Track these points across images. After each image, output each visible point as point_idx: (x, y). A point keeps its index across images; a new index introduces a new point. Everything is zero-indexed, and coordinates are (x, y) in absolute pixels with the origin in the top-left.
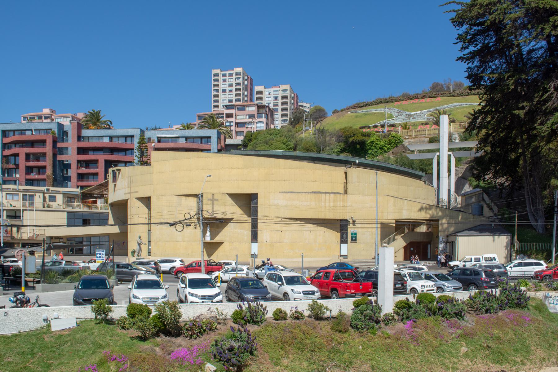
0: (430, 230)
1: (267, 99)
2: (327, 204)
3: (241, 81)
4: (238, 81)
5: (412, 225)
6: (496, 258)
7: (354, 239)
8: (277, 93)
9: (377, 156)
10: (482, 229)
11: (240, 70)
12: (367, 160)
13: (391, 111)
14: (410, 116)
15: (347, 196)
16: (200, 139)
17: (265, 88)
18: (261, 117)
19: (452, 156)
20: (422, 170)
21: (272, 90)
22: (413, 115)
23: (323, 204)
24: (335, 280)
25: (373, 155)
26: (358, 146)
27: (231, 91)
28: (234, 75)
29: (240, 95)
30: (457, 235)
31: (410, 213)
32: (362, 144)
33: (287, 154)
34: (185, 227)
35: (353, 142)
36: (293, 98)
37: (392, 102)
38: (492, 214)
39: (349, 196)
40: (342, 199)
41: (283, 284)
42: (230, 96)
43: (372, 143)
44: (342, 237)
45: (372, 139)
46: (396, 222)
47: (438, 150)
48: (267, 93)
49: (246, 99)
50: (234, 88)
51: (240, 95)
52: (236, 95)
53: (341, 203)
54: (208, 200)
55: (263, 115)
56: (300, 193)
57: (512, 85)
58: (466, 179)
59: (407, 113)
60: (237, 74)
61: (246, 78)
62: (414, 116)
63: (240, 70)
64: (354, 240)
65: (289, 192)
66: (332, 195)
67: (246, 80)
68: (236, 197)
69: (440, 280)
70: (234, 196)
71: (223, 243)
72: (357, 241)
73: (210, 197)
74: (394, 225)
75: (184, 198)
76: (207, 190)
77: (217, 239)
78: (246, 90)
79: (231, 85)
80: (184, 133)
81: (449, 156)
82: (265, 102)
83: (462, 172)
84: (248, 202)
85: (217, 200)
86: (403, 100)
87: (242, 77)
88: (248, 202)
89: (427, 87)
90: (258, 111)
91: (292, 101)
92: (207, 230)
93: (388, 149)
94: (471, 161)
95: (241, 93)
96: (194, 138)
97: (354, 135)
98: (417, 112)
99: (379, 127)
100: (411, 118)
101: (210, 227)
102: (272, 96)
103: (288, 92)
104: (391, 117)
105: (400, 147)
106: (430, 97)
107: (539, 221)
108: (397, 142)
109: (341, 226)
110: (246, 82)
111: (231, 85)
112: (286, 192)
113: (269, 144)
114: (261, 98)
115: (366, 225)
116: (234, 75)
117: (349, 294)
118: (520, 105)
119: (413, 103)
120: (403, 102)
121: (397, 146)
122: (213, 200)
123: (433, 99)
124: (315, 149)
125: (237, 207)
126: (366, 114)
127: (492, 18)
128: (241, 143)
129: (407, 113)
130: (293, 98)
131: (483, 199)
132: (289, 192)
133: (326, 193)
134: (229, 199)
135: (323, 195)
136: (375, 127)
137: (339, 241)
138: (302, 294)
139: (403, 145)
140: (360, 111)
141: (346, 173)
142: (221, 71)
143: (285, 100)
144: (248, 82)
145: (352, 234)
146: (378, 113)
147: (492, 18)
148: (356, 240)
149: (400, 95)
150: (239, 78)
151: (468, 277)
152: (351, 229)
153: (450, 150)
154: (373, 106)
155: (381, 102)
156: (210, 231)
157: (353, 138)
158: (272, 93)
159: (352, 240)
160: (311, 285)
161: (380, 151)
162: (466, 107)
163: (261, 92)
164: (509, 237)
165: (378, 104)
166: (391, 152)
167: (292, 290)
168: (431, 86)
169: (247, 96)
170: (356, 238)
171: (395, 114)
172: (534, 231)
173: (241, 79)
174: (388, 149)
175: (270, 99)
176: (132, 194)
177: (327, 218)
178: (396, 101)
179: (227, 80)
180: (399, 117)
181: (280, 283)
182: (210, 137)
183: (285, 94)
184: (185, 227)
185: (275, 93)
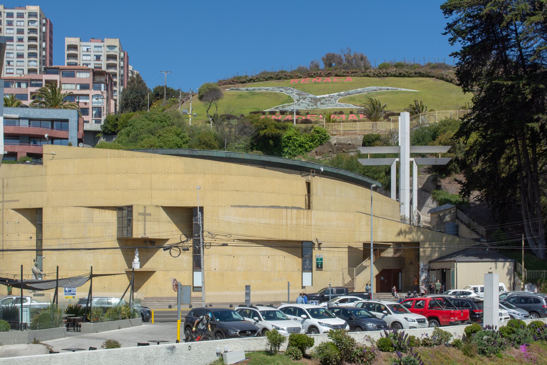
0: (398, 255)
1: (85, 58)
2: (289, 222)
3: (36, 26)
4: (32, 26)
5: (380, 247)
6: (504, 287)
7: (320, 266)
8: (100, 49)
9: (295, 156)
10: (478, 253)
11: (35, 9)
12: (285, 160)
13: (288, 91)
14: (316, 101)
15: (311, 212)
16: (50, 122)
17: (81, 41)
18: (100, 89)
19: (414, 163)
20: (379, 180)
21: (92, 44)
22: (320, 100)
23: (284, 222)
24: (430, 308)
25: (290, 154)
26: (271, 142)
27: (21, 40)
28: (26, 16)
29: (35, 47)
30: (455, 261)
31: (388, 233)
32: (277, 139)
33: (232, 156)
34: (182, 251)
35: (265, 135)
36: (122, 59)
37: (286, 79)
38: (475, 236)
39: (314, 213)
40: (305, 215)
41: (260, 319)
42: (19, 48)
43: (289, 138)
44: (303, 264)
45: (289, 133)
46: (364, 244)
47: (397, 155)
48: (85, 49)
49: (44, 53)
50: (26, 36)
51: (35, 47)
52: (30, 47)
53: (305, 221)
54: (139, 214)
55: (103, 85)
56: (256, 207)
57: (529, 94)
58: (429, 192)
59: (311, 96)
60: (30, 15)
61: (44, 21)
62: (322, 101)
63: (35, 9)
64: (320, 267)
65: (242, 206)
66: (295, 211)
67: (44, 25)
68: (173, 212)
69: (313, 317)
70: (169, 210)
71: (153, 272)
72: (324, 269)
73: (141, 210)
74: (362, 249)
75: (98, 210)
76: (138, 203)
77: (148, 266)
78: (44, 41)
79: (20, 31)
80: (26, 113)
81: (411, 163)
82: (82, 63)
83: (423, 183)
84: (188, 218)
85: (150, 215)
86: (300, 77)
87: (38, 19)
88: (188, 218)
89: (316, 57)
90: (94, 80)
91: (122, 63)
92: (134, 255)
93: (310, 147)
94: (429, 169)
95: (38, 44)
96: (40, 120)
97: (266, 126)
98: (325, 96)
99: (278, 113)
100: (319, 103)
101: (139, 251)
102: (92, 54)
103: (117, 49)
104: (290, 100)
105: (325, 145)
106: (336, 76)
107: (540, 245)
108: (321, 139)
109: (302, 249)
110: (44, 29)
111: (20, 31)
112: (239, 206)
113: (157, 135)
114: (75, 56)
115: (332, 249)
116: (26, 16)
117: (452, 321)
118: (536, 117)
119: (315, 83)
120: (302, 80)
121: (321, 144)
122: (145, 214)
123: (343, 79)
124: (216, 144)
125: (173, 224)
126: (253, 94)
127: (509, 18)
128: (100, 129)
129: (311, 96)
130: (122, 59)
131: (457, 218)
132: (242, 206)
133: (286, 208)
134: (164, 215)
135: (284, 210)
136: (273, 113)
137: (301, 270)
138: (416, 322)
139: (329, 143)
140: (243, 89)
141: (308, 184)
142: (5, 8)
143: (111, 62)
144: (46, 29)
145: (317, 259)
146: (271, 93)
147: (509, 18)
148: (321, 267)
149: (293, 69)
150: (35, 21)
151: (532, 305)
152: (316, 253)
153: (412, 155)
154: (260, 83)
155: (272, 78)
156: (138, 256)
157: (265, 131)
158: (92, 49)
159: (317, 267)
160: (337, 318)
161: (300, 149)
162: (389, 93)
163: (75, 47)
164: (512, 263)
165: (267, 80)
166: (313, 151)
167: (406, 319)
168: (324, 56)
169: (45, 49)
170: (322, 264)
171: (295, 97)
172: (534, 256)
173: (37, 24)
174: (310, 147)
175: (88, 58)
176: (5, 204)
177: (289, 239)
178: (291, 78)
179: (15, 23)
180: (302, 100)
181: (256, 318)
182: (67, 121)
183: (112, 53)
184: (182, 251)
185: (96, 49)
